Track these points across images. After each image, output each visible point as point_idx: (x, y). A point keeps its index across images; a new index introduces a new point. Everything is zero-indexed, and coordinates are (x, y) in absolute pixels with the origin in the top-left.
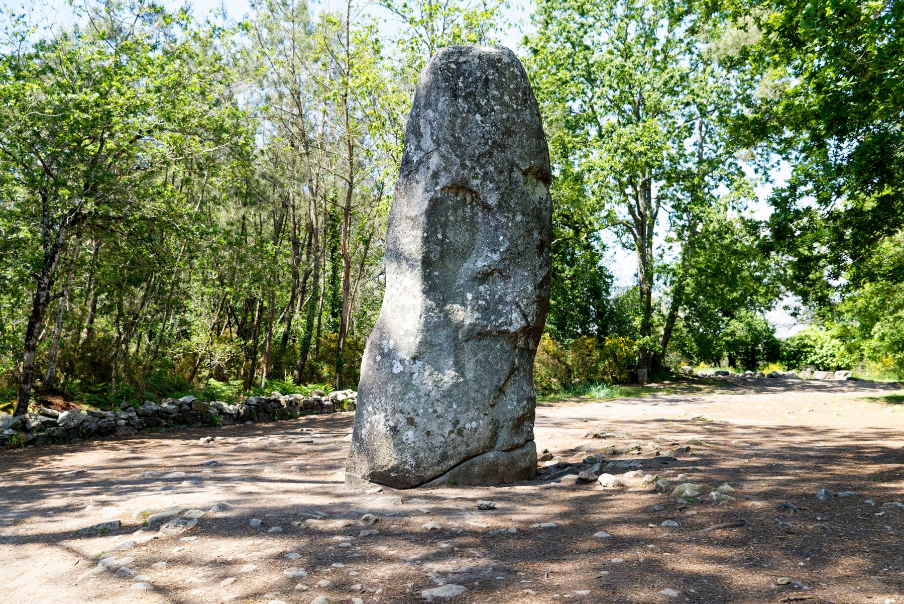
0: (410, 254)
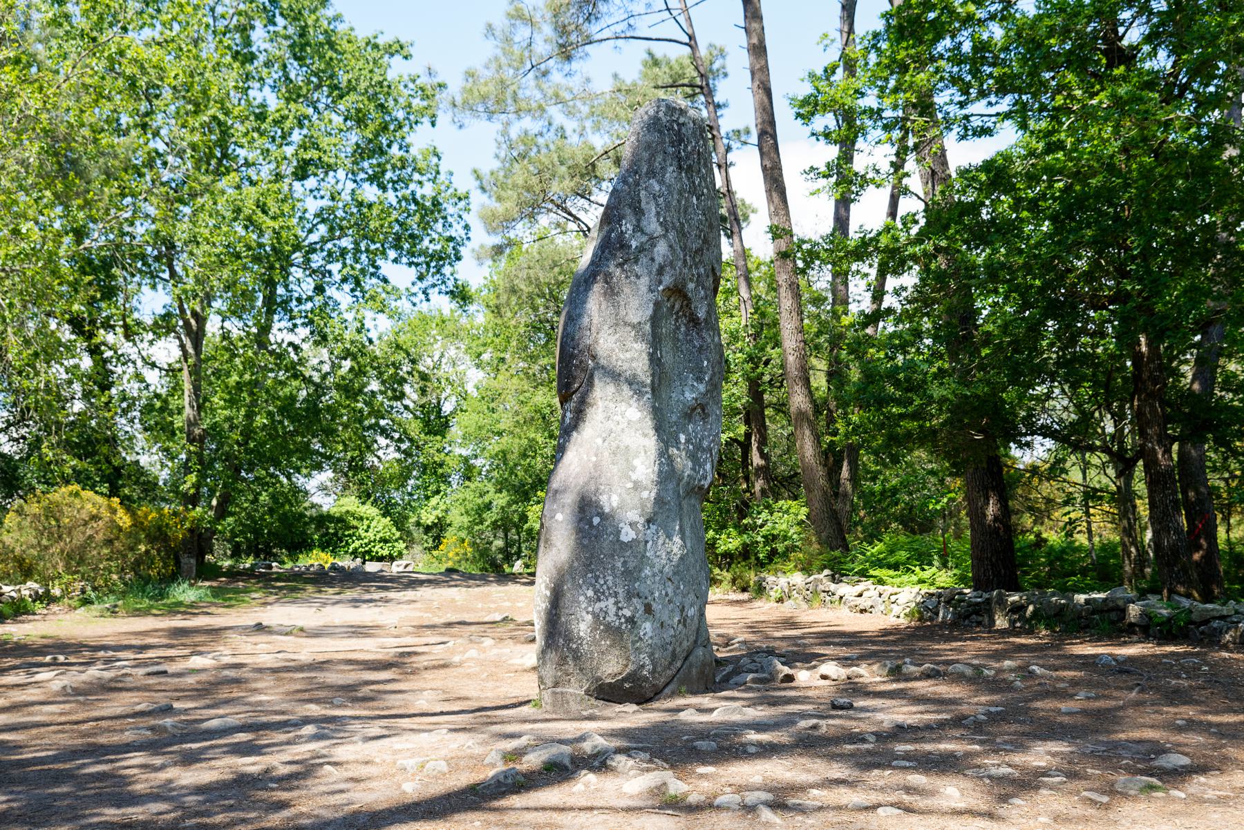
0: (635, 375)
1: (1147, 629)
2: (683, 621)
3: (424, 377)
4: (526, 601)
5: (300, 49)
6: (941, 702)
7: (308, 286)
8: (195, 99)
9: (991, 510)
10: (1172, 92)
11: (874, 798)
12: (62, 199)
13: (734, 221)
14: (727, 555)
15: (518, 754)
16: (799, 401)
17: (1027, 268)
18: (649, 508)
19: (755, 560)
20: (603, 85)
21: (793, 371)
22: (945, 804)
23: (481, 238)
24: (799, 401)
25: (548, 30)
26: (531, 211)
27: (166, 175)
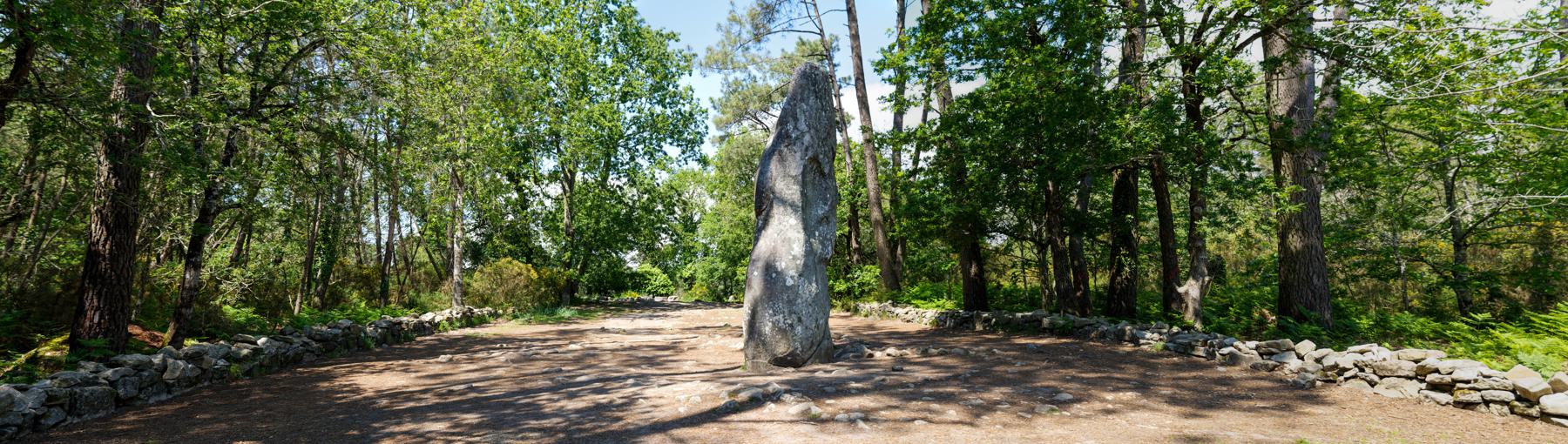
1: (1052, 331)
2: (817, 327)
3: (685, 203)
4: (738, 316)
5: (624, 37)
6: (948, 368)
7: (627, 157)
8: (570, 60)
9: (973, 270)
10: (1065, 58)
11: (913, 415)
12: (504, 114)
13: (843, 124)
14: (839, 293)
15: (736, 392)
16: (876, 215)
17: (991, 147)
19: (852, 296)
20: (777, 55)
21: (873, 200)
22: (949, 418)
23: (714, 132)
24: (876, 215)
25: (749, 27)
26: (739, 117)
27: (556, 100)
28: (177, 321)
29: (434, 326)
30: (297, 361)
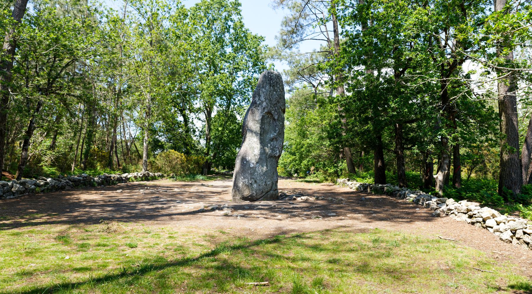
18: (257, 160)
28: (19, 171)
29: (127, 179)
30: (63, 188)
